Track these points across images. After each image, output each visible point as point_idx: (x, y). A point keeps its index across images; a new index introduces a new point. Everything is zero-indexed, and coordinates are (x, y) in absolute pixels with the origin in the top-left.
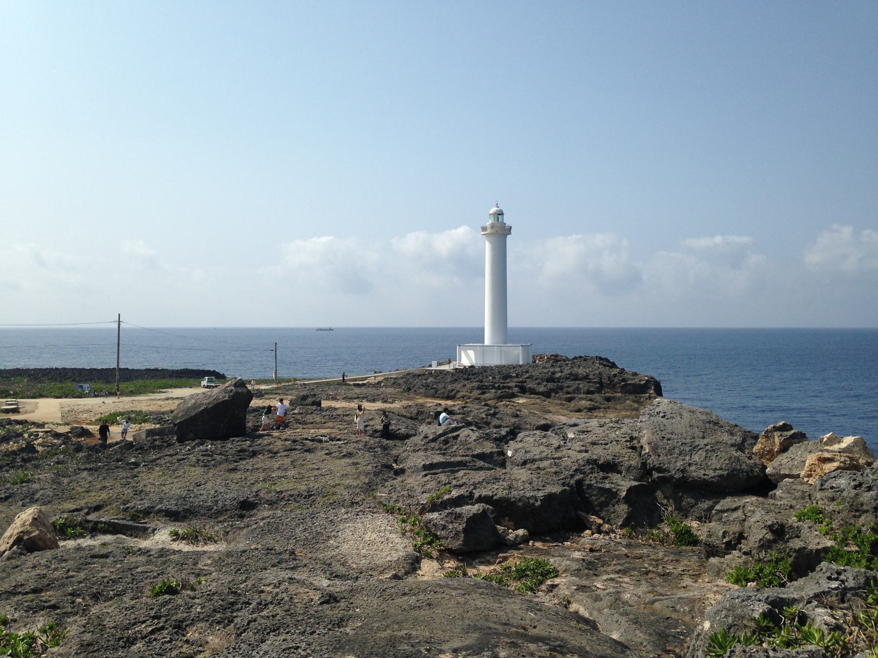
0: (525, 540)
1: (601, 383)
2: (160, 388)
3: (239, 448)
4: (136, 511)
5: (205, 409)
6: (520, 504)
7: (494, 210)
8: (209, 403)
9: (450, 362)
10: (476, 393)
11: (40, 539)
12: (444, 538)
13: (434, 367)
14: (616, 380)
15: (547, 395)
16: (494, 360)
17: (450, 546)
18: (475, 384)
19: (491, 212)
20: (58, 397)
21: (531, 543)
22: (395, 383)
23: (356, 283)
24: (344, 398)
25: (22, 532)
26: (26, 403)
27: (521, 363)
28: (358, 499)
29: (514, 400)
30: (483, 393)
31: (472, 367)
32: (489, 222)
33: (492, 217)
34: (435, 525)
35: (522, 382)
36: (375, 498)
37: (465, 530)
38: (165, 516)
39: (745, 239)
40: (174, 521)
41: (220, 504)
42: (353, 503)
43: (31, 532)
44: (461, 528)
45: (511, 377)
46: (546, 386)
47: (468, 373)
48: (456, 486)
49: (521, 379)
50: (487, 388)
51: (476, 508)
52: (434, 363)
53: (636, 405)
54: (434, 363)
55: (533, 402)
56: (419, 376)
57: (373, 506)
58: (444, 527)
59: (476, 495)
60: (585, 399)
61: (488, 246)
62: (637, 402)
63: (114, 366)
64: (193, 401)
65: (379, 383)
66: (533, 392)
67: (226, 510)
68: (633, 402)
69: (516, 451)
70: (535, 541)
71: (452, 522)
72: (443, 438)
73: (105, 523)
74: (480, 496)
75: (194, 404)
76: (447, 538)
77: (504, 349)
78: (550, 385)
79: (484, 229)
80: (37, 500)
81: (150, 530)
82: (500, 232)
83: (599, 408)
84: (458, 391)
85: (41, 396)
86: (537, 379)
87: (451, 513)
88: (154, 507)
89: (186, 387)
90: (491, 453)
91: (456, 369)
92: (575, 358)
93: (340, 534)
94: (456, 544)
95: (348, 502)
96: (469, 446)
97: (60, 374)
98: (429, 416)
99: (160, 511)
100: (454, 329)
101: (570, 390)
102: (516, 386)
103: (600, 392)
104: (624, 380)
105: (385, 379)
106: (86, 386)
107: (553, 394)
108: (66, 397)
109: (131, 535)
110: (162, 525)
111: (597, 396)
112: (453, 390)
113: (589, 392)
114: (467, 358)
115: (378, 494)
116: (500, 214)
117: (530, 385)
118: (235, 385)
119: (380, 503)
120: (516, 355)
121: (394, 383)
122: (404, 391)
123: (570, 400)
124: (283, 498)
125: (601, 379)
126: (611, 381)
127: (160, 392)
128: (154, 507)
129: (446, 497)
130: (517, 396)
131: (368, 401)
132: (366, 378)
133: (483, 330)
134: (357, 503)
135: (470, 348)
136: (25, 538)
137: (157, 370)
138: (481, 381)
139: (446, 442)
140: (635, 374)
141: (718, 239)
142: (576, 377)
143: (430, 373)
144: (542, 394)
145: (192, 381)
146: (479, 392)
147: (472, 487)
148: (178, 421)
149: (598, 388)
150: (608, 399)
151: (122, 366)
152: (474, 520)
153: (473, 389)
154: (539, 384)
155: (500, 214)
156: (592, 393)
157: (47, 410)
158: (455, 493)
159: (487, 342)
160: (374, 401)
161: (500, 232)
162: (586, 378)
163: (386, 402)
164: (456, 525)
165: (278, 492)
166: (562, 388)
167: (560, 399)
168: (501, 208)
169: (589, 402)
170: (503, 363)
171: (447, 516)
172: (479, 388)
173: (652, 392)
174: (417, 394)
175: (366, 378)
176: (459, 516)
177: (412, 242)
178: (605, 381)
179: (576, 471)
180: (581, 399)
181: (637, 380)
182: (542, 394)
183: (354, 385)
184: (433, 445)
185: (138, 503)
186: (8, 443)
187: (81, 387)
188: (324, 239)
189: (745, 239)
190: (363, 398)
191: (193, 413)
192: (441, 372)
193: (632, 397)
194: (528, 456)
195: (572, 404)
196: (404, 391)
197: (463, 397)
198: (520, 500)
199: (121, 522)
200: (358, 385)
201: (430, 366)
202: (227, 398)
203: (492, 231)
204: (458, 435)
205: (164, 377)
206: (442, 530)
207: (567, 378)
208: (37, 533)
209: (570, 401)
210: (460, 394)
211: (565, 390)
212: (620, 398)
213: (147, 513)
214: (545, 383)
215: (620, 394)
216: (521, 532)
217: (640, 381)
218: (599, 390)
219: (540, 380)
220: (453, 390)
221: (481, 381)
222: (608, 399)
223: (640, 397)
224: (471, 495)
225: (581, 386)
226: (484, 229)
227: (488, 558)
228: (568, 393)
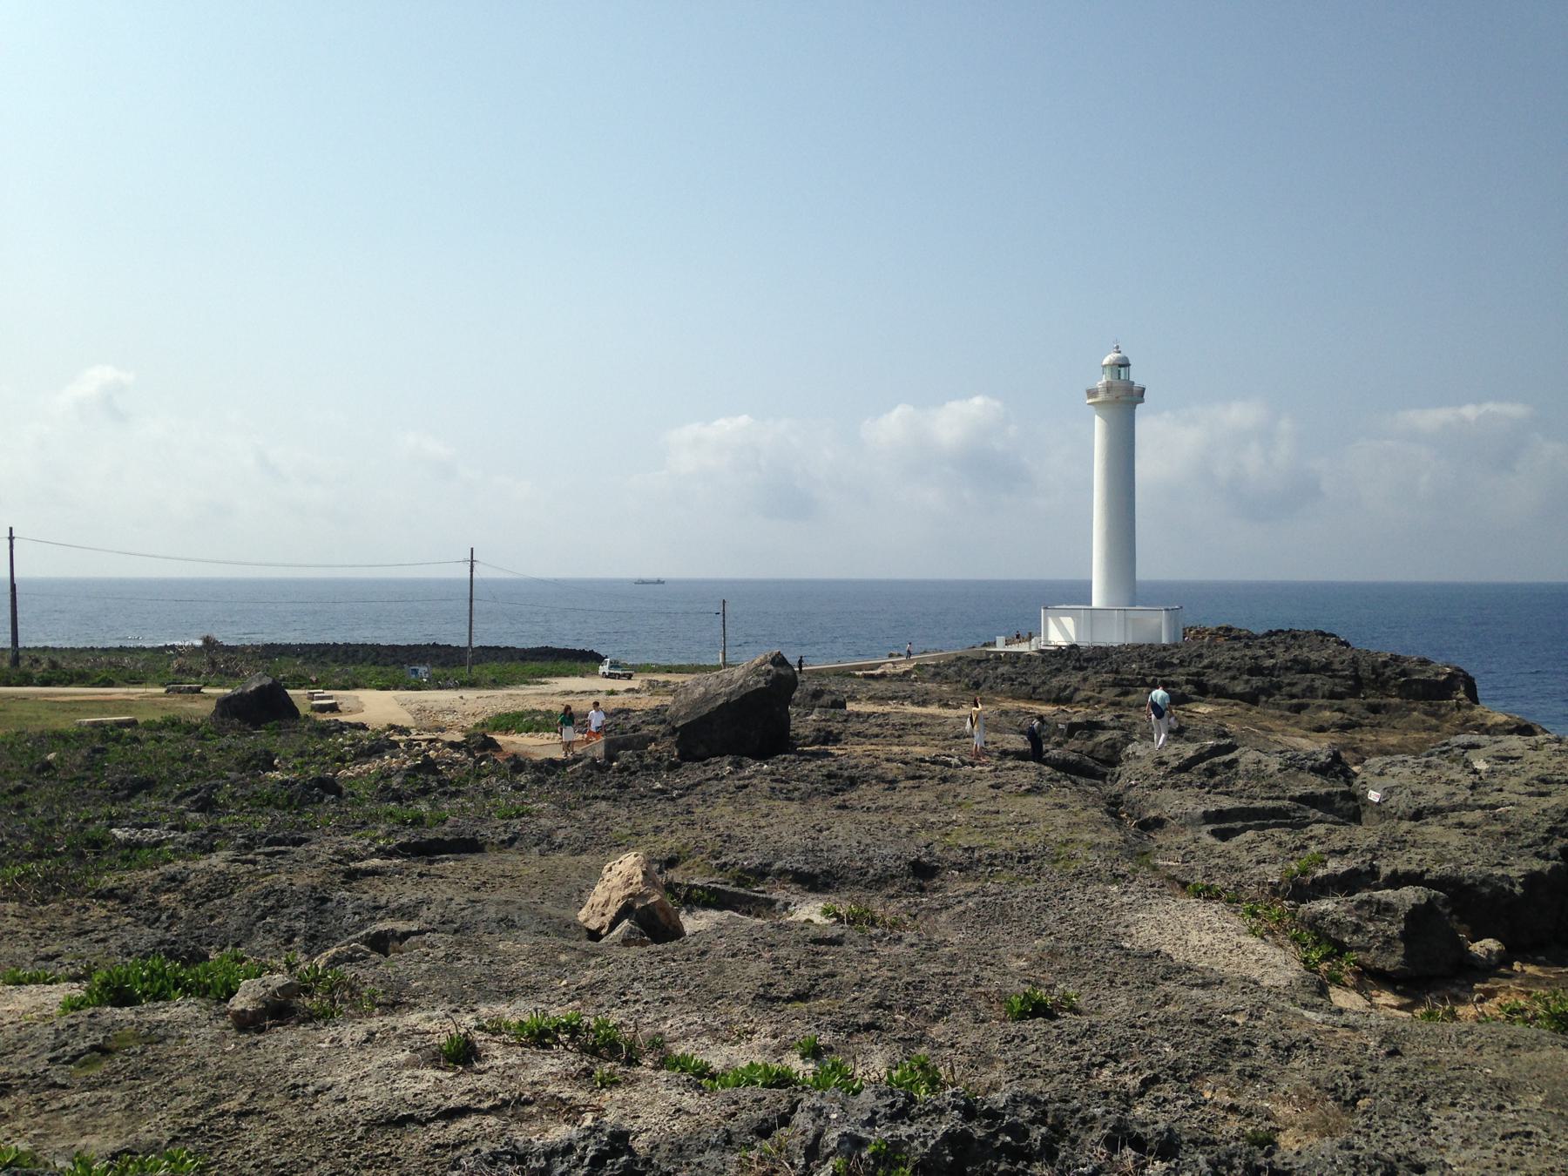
0: (1505, 959)
1: (1356, 678)
2: (533, 675)
3: (825, 771)
4: (742, 870)
5: (727, 704)
6: (1486, 890)
7: (1109, 358)
8: (731, 694)
9: (1030, 637)
10: (1110, 694)
11: (662, 909)
12: (1359, 948)
13: (1000, 647)
14: (1388, 672)
15: (1251, 699)
16: (1112, 636)
17: (1379, 965)
18: (1110, 677)
19: (1106, 361)
20: (383, 689)
21: (1517, 966)
22: (938, 673)
23: (790, 500)
24: (870, 698)
25: (630, 895)
26: (342, 697)
27: (1165, 641)
28: (1123, 869)
29: (1187, 706)
30: (1126, 694)
31: (1073, 647)
32: (1102, 381)
33: (1107, 371)
34: (1336, 923)
35: (1198, 674)
36: (1155, 868)
37: (1404, 936)
38: (793, 881)
39: (1516, 410)
40: (809, 891)
41: (878, 865)
42: (1116, 876)
43: (647, 897)
44: (1395, 930)
45: (1171, 665)
46: (1247, 682)
47: (1070, 657)
48: (1334, 853)
49: (1194, 670)
50: (1131, 684)
51: (1410, 895)
52: (1000, 640)
53: (1434, 722)
54: (1000, 640)
55: (1227, 711)
56: (979, 662)
57: (1158, 883)
58: (1357, 929)
59: (1385, 871)
60: (1330, 708)
61: (1099, 424)
62: (1434, 715)
63: (464, 643)
64: (702, 689)
65: (907, 673)
66: (1221, 693)
67: (893, 877)
68: (1426, 713)
69: (1389, 791)
70: (1524, 961)
71: (1371, 920)
72: (1203, 765)
73: (702, 888)
74: (1395, 872)
75: (706, 693)
76: (1368, 950)
77: (1131, 615)
78: (1257, 681)
79: (1092, 393)
80: (560, 846)
81: (778, 906)
82: (1124, 399)
83: (1361, 726)
84: (1077, 690)
85: (356, 686)
86: (1228, 669)
87: (1369, 902)
88: (770, 865)
89: (575, 675)
90: (1328, 794)
91: (1042, 651)
92: (1270, 634)
93: (1133, 930)
94: (1392, 961)
95: (1105, 875)
96: (1271, 781)
97: (346, 652)
98: (1056, 731)
99: (782, 872)
100: (1006, 584)
101: (1295, 690)
102: (1187, 682)
103: (1355, 696)
104: (1404, 673)
105: (917, 667)
106: (422, 669)
107: (1264, 699)
108: (396, 688)
109: (749, 913)
110: (796, 898)
111: (1350, 703)
112: (1066, 687)
113: (1332, 695)
114: (1059, 632)
115: (1160, 862)
116: (1124, 364)
117: (1215, 679)
118: (773, 662)
119: (1171, 878)
120: (1157, 628)
121: (936, 674)
122: (968, 688)
123: (1298, 709)
124: (979, 860)
125: (1356, 670)
126: (1378, 675)
127: (538, 683)
128: (770, 865)
129: (1320, 873)
130: (1192, 701)
131: (913, 703)
132: (878, 666)
133: (1089, 584)
134: (1124, 876)
135: (1067, 612)
136: (638, 905)
137: (497, 648)
138: (1117, 672)
139: (1211, 772)
140: (1424, 662)
141: (1469, 411)
142: (1305, 667)
143: (997, 656)
144: (1241, 697)
145: (585, 667)
146: (1118, 690)
147: (1369, 856)
148: (680, 723)
149: (1351, 687)
150: (1375, 709)
151: (475, 644)
152: (1418, 917)
153: (1102, 686)
154: (1234, 678)
155: (1124, 364)
156: (1341, 696)
157: (377, 707)
158: (1335, 866)
159: (1096, 602)
160: (924, 703)
161: (1124, 399)
162: (1326, 668)
163: (946, 705)
164: (1383, 925)
165: (966, 850)
166: (1279, 688)
167: (1278, 706)
168: (1125, 353)
169: (1338, 715)
170: (1130, 641)
171: (1357, 908)
172: (1115, 684)
173: (1461, 695)
174: (997, 694)
175: (878, 666)
176: (1386, 908)
177: (891, 426)
178: (1366, 672)
179: (1551, 830)
180: (1320, 708)
181: (1429, 674)
182: (1241, 697)
183: (866, 676)
184: (1185, 777)
185: (741, 855)
186: (382, 758)
187: (416, 671)
188: (724, 426)
189: (1516, 410)
190: (905, 698)
191: (706, 710)
192: (1018, 655)
193: (1422, 705)
194: (1423, 801)
195: (1304, 716)
196: (968, 688)
197: (1087, 700)
198: (1484, 882)
199: (729, 888)
200: (872, 677)
201: (994, 644)
202: (762, 685)
203: (1108, 397)
204: (1235, 761)
205: (512, 659)
206: (1354, 933)
207: (1288, 669)
208: (656, 898)
209: (1298, 712)
210: (1081, 695)
211: (1286, 690)
212: (1398, 708)
213: (761, 873)
214: (1246, 677)
215: (1397, 700)
216: (1491, 944)
217: (1437, 674)
218: (1354, 692)
219: (1237, 672)
220: (1066, 687)
221: (1117, 672)
222: (1375, 709)
223: (1440, 706)
224: (1373, 872)
225: (1318, 683)
226: (1092, 393)
227: (1455, 990)
228: (1292, 696)
